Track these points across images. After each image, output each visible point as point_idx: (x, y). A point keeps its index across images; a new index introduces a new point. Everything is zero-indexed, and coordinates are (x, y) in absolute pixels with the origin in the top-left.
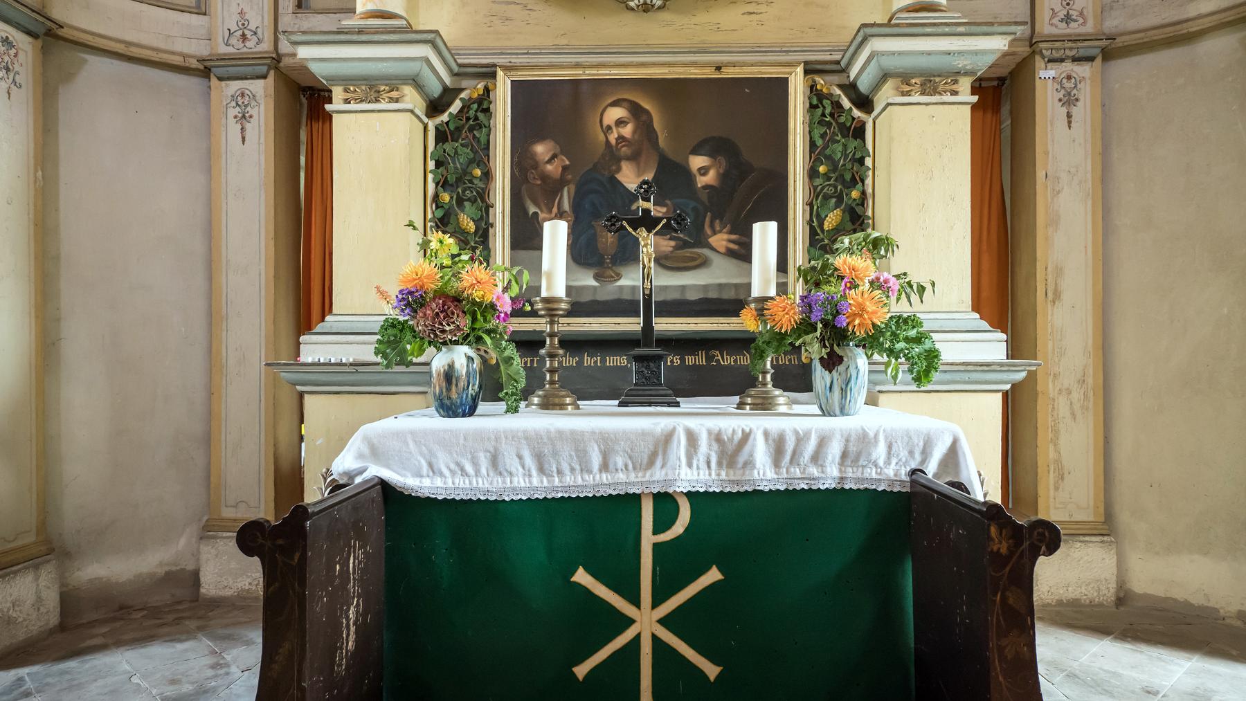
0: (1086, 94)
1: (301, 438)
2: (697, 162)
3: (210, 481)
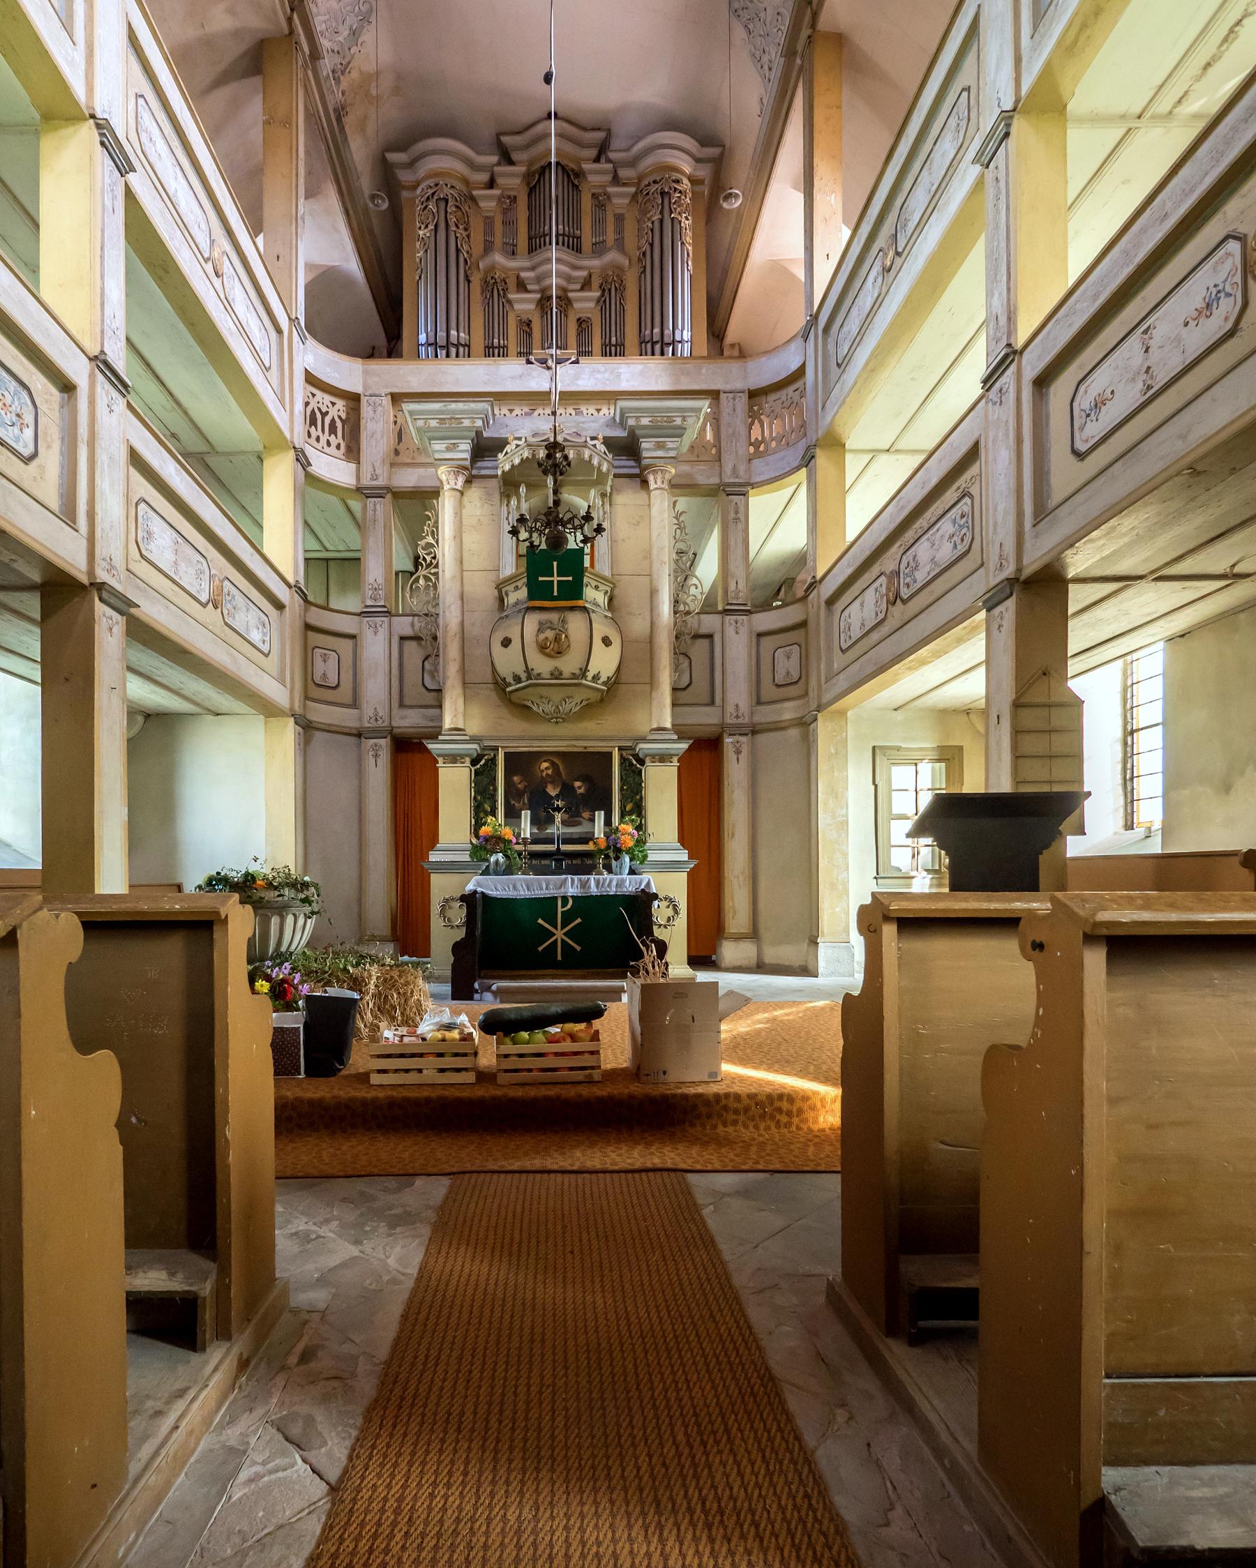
0: (745, 750)
2: (577, 784)
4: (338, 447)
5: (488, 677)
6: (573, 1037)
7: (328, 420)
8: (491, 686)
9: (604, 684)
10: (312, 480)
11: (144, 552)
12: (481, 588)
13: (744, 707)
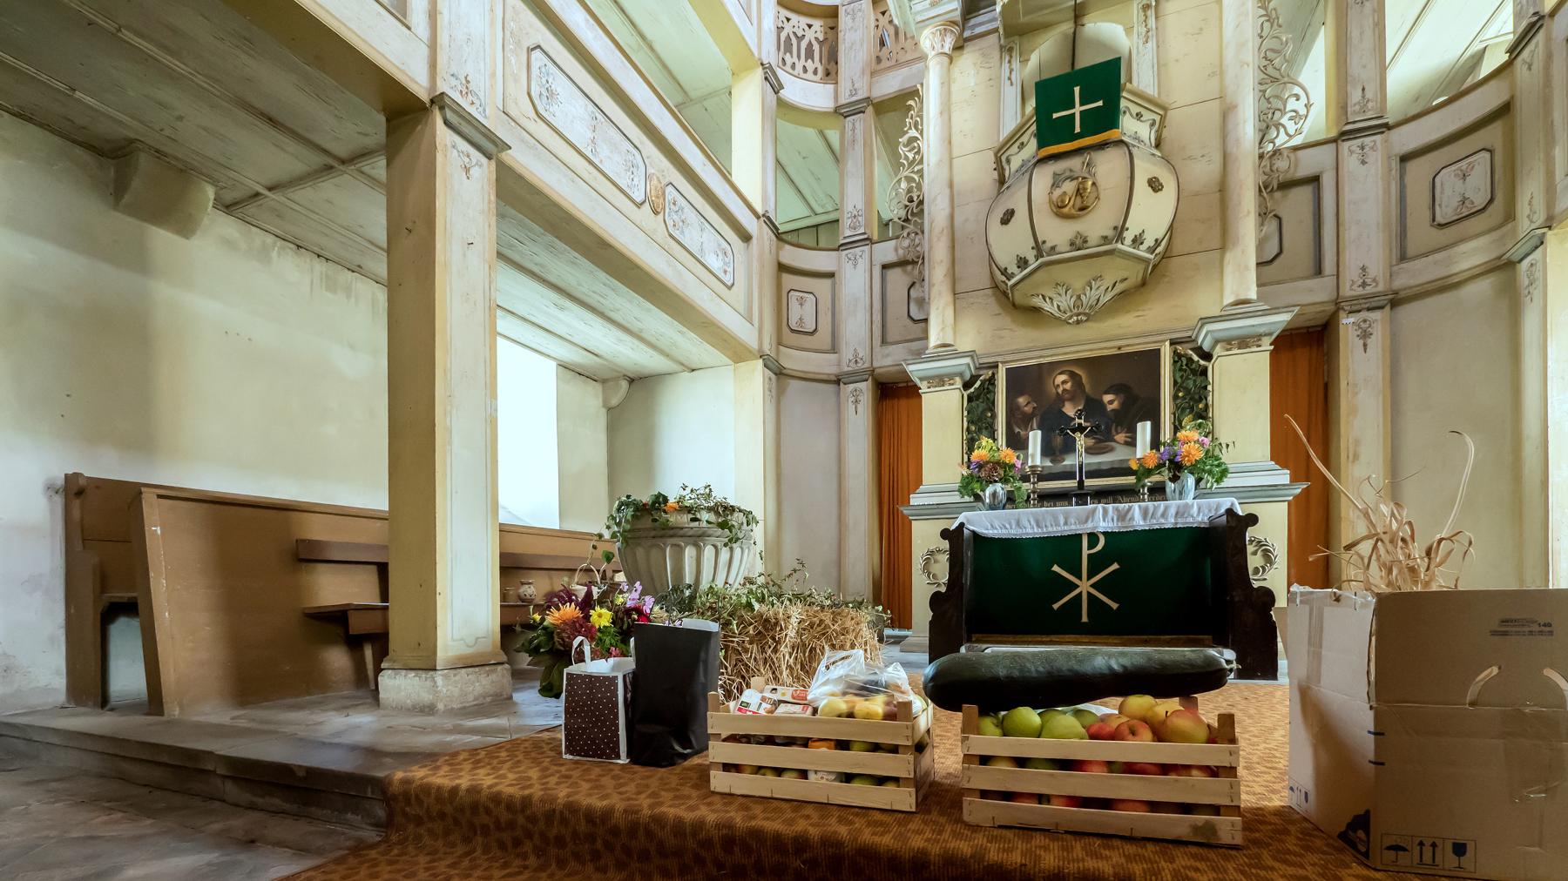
1: (1510, 51)
2: (1107, 398)
3: (840, 584)
4: (815, 72)
5: (987, 283)
6: (1160, 732)
7: (804, 44)
8: (989, 292)
9: (1151, 250)
10: (785, 108)
11: (542, 111)
12: (975, 171)
13: (1377, 269)
